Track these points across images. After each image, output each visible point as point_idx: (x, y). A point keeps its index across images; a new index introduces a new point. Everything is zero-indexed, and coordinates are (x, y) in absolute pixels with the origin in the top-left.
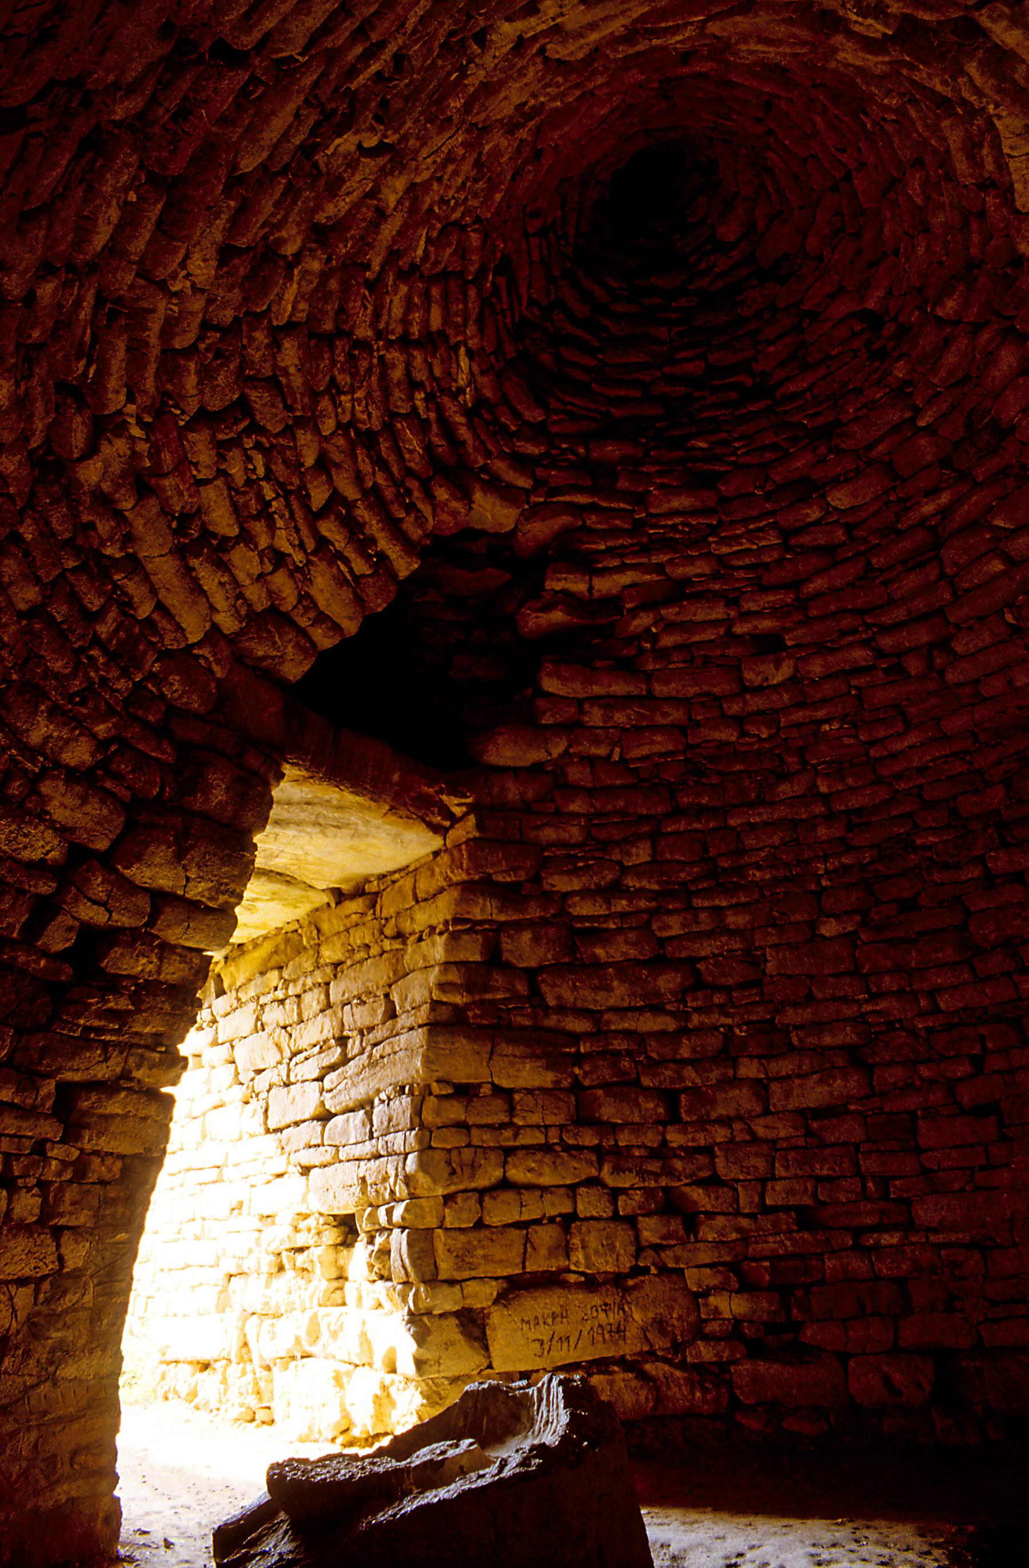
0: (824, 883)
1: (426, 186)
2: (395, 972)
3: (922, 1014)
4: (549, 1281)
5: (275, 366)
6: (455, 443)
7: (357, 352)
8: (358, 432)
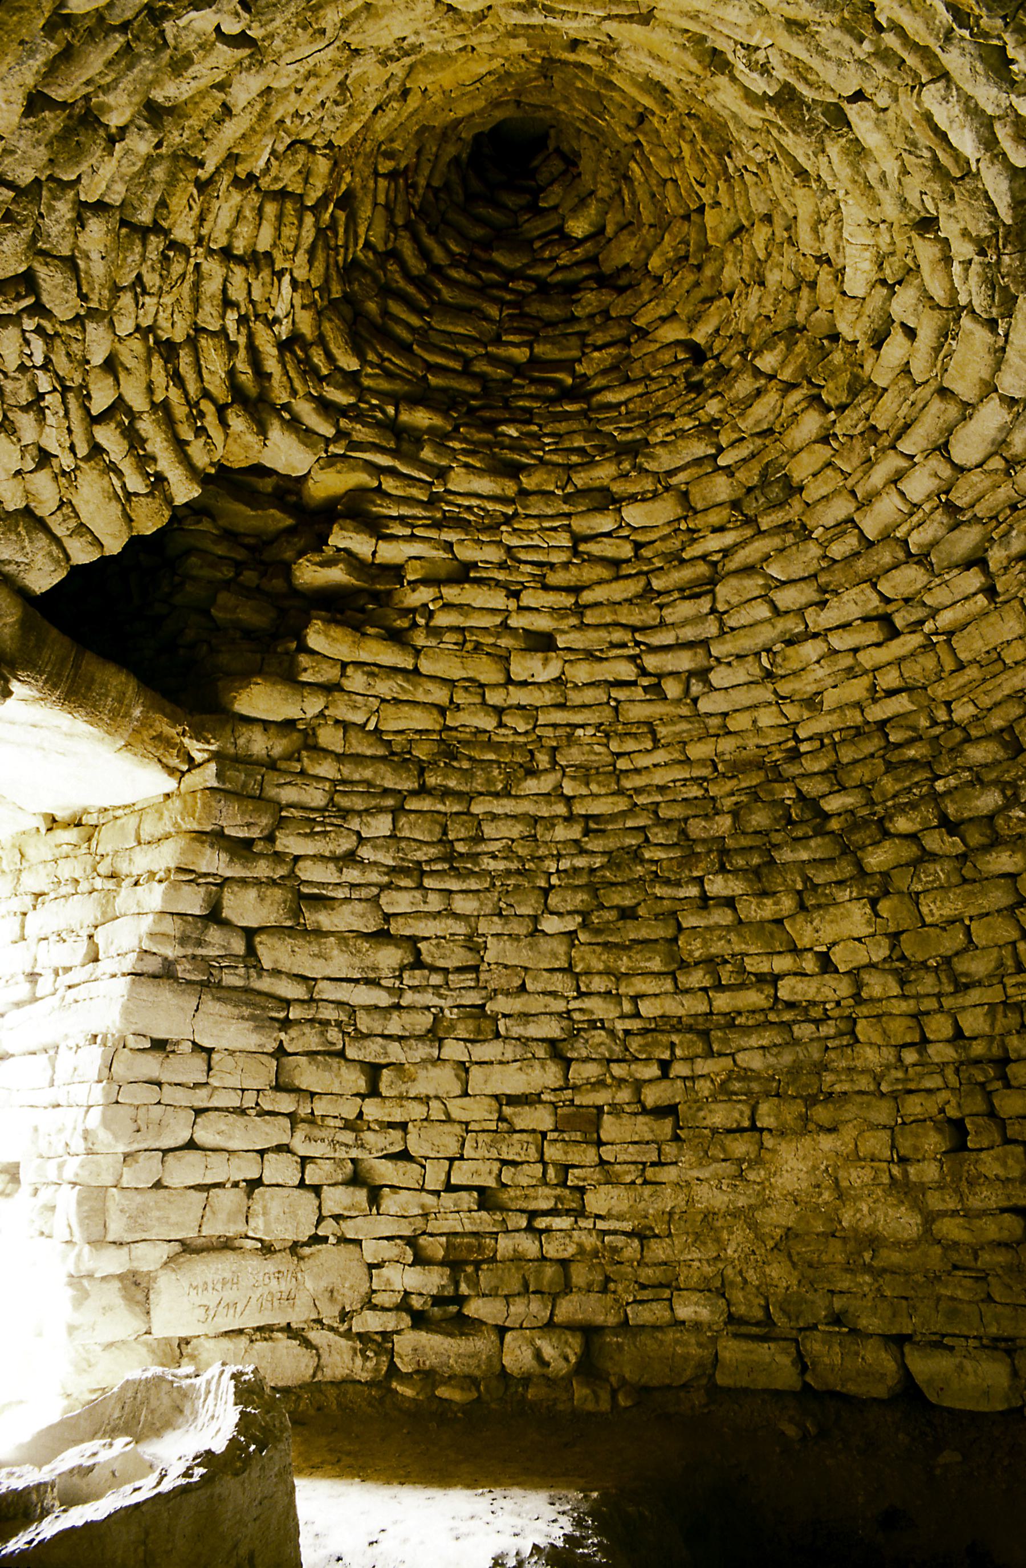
0: (554, 880)
1: (283, 93)
2: (104, 913)
3: (623, 1017)
4: (226, 1245)
5: (75, 246)
6: (261, 375)
7: (171, 254)
8: (158, 341)
